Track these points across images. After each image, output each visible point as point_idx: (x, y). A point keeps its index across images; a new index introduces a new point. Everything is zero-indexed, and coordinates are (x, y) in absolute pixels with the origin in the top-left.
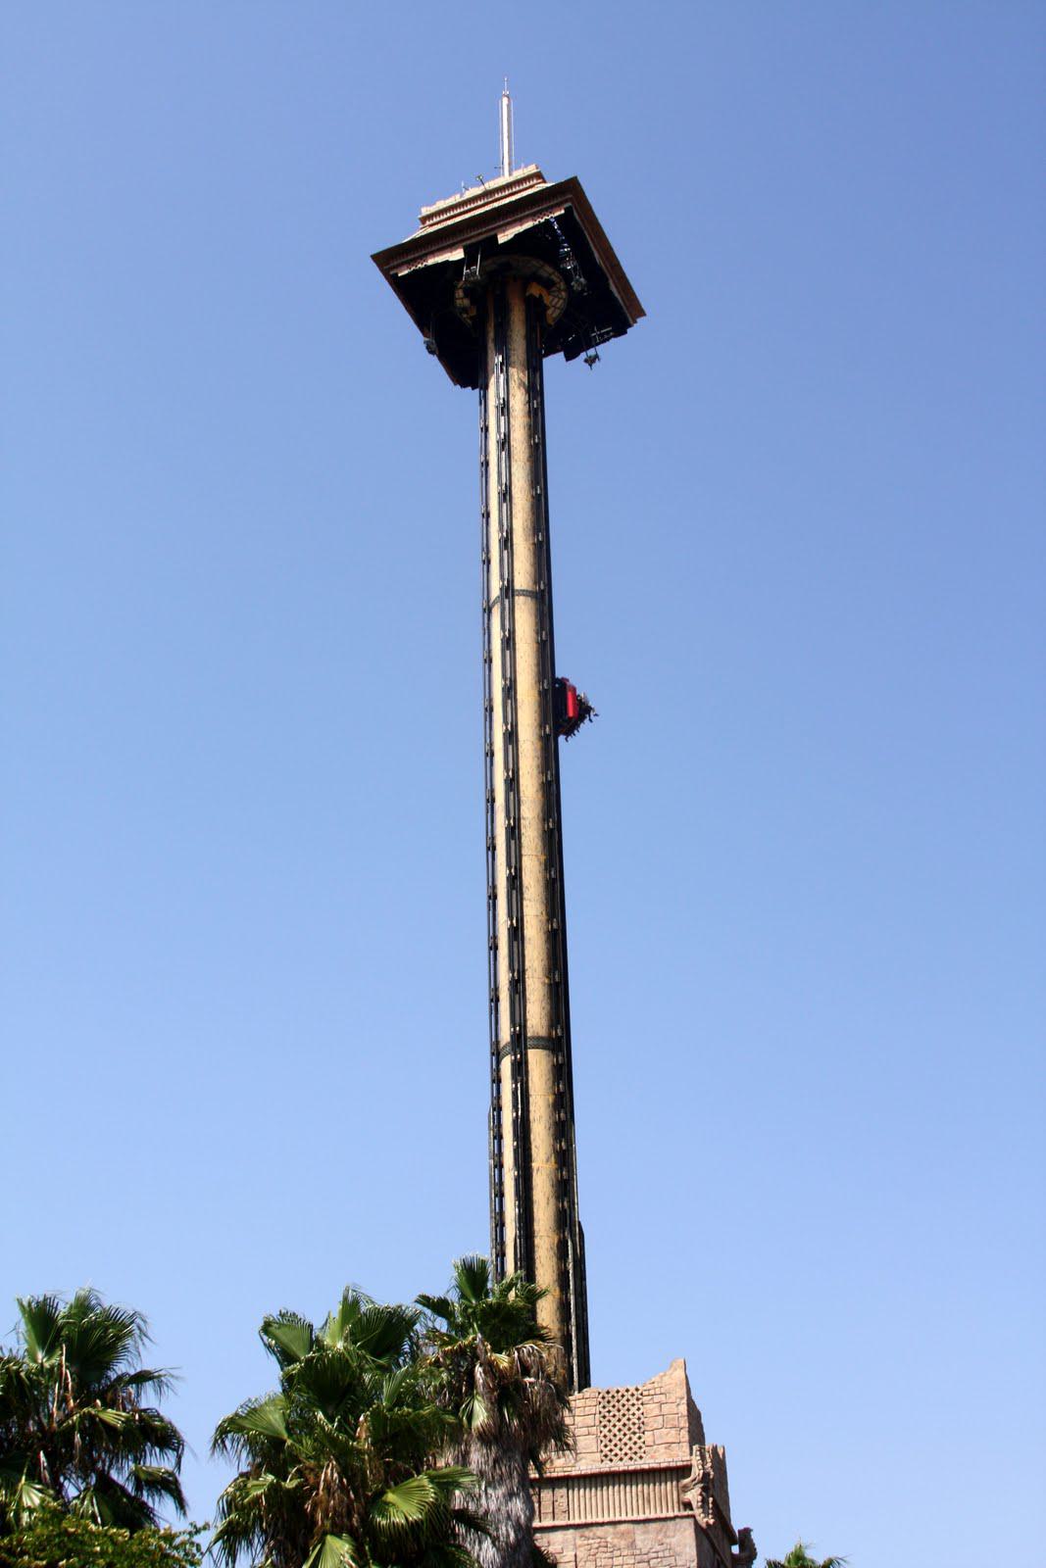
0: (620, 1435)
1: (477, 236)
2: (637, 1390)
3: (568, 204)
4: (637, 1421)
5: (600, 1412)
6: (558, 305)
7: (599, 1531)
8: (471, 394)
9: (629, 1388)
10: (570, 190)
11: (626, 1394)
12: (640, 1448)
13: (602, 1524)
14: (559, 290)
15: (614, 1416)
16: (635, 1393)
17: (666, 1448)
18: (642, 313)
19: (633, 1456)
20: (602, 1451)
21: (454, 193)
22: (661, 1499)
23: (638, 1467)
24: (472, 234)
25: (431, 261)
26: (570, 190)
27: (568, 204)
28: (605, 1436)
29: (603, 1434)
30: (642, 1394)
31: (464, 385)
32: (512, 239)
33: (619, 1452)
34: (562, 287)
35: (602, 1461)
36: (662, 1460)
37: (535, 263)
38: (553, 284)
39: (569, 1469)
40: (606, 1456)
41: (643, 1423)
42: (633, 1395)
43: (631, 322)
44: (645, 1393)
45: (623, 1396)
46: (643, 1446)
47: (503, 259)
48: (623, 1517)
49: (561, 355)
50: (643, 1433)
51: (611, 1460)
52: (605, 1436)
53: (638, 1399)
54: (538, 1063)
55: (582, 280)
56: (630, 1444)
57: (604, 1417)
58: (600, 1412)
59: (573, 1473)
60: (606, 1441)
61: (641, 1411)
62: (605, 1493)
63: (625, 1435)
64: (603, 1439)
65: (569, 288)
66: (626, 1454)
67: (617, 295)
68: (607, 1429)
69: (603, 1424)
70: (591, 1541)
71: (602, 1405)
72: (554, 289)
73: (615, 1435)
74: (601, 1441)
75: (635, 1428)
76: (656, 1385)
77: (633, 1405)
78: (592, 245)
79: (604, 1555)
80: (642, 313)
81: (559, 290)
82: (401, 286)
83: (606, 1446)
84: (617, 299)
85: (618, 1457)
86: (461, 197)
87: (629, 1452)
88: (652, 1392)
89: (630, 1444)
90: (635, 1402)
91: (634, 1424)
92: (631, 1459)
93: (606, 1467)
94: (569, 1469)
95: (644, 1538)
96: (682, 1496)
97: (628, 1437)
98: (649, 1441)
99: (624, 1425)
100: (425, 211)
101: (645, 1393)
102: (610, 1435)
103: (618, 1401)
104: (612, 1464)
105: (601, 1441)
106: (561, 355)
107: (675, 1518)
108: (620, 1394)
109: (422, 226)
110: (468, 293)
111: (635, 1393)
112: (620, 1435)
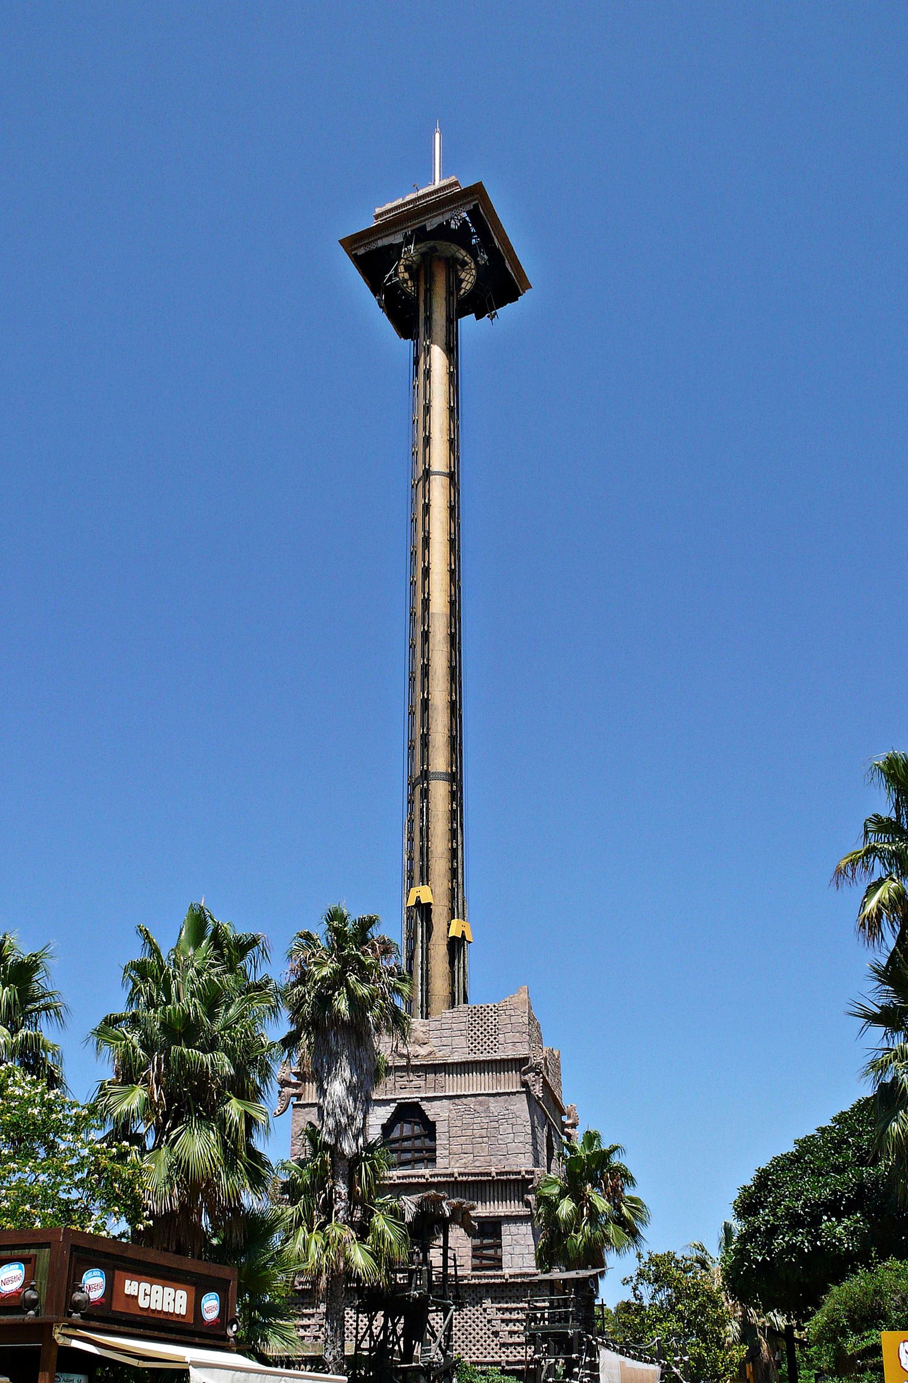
0: (481, 1036)
1: (416, 224)
2: (495, 1006)
3: (476, 202)
4: (493, 1027)
5: (469, 1021)
6: (470, 281)
7: (464, 1100)
8: (409, 343)
9: (489, 1005)
10: (478, 191)
11: (487, 1009)
12: (495, 1045)
13: (466, 1096)
14: (471, 269)
15: (478, 1023)
16: (493, 1008)
17: (512, 1046)
18: (529, 287)
19: (490, 1050)
20: (469, 1047)
21: (399, 198)
22: (510, 1081)
23: (494, 1058)
24: (409, 224)
25: (380, 243)
26: (478, 191)
27: (476, 202)
28: (472, 1037)
29: (470, 1036)
30: (497, 1009)
31: (406, 338)
32: (437, 227)
33: (480, 1048)
34: (473, 267)
35: (469, 1053)
36: (509, 1053)
37: (454, 247)
38: (466, 264)
39: (446, 1058)
40: (472, 1050)
41: (498, 1029)
42: (478, 1011)
43: (522, 292)
44: (499, 1009)
45: (485, 1010)
46: (497, 1044)
47: (431, 243)
48: (483, 1092)
49: (473, 316)
50: (498, 1035)
51: (475, 1053)
52: (472, 1037)
53: (495, 1013)
54: (439, 790)
55: (486, 257)
56: (488, 1042)
57: (472, 1024)
58: (469, 1021)
59: (449, 1061)
60: (472, 1040)
61: (496, 1021)
62: (487, 1076)
63: (485, 1036)
64: (470, 1039)
65: (476, 263)
66: (485, 1049)
67: (511, 271)
68: (473, 1032)
69: (470, 1029)
70: (459, 1107)
71: (470, 1016)
72: (467, 267)
73: (478, 1037)
74: (469, 1040)
75: (492, 1032)
76: (508, 1003)
77: (492, 1016)
78: (492, 232)
79: (468, 1116)
80: (529, 287)
81: (471, 269)
82: (360, 261)
83: (472, 1044)
84: (511, 273)
85: (480, 1051)
86: (403, 200)
87: (487, 1048)
88: (505, 1008)
89: (488, 1042)
90: (493, 1014)
91: (492, 1029)
92: (489, 1052)
93: (471, 1057)
94: (446, 1058)
95: (495, 1105)
96: (522, 1077)
97: (487, 1038)
98: (502, 1040)
99: (485, 1030)
100: (378, 210)
101: (499, 1009)
102: (475, 1037)
103: (481, 1014)
104: (475, 1056)
105: (469, 1040)
106: (473, 316)
107: (518, 1092)
108: (483, 1009)
109: (375, 221)
110: (407, 268)
111: (493, 1008)
112: (481, 1036)
